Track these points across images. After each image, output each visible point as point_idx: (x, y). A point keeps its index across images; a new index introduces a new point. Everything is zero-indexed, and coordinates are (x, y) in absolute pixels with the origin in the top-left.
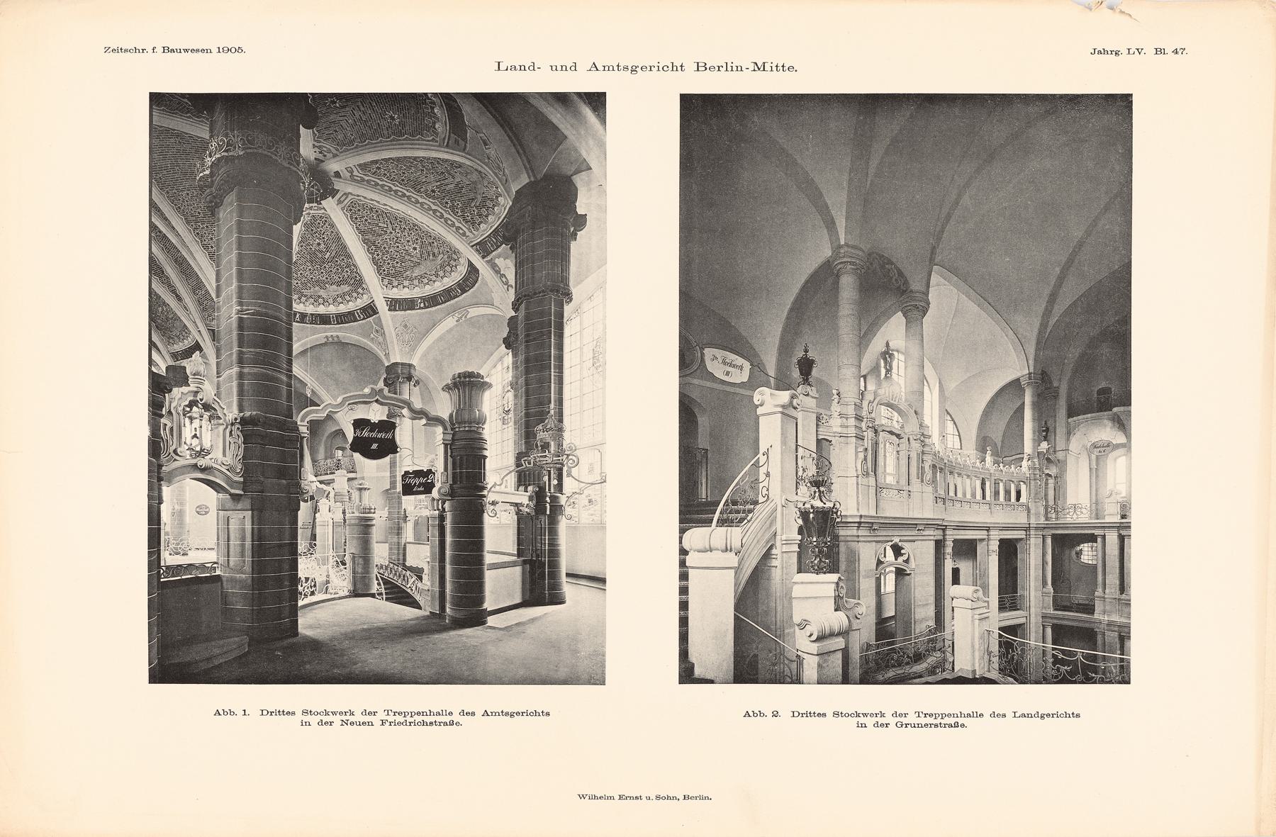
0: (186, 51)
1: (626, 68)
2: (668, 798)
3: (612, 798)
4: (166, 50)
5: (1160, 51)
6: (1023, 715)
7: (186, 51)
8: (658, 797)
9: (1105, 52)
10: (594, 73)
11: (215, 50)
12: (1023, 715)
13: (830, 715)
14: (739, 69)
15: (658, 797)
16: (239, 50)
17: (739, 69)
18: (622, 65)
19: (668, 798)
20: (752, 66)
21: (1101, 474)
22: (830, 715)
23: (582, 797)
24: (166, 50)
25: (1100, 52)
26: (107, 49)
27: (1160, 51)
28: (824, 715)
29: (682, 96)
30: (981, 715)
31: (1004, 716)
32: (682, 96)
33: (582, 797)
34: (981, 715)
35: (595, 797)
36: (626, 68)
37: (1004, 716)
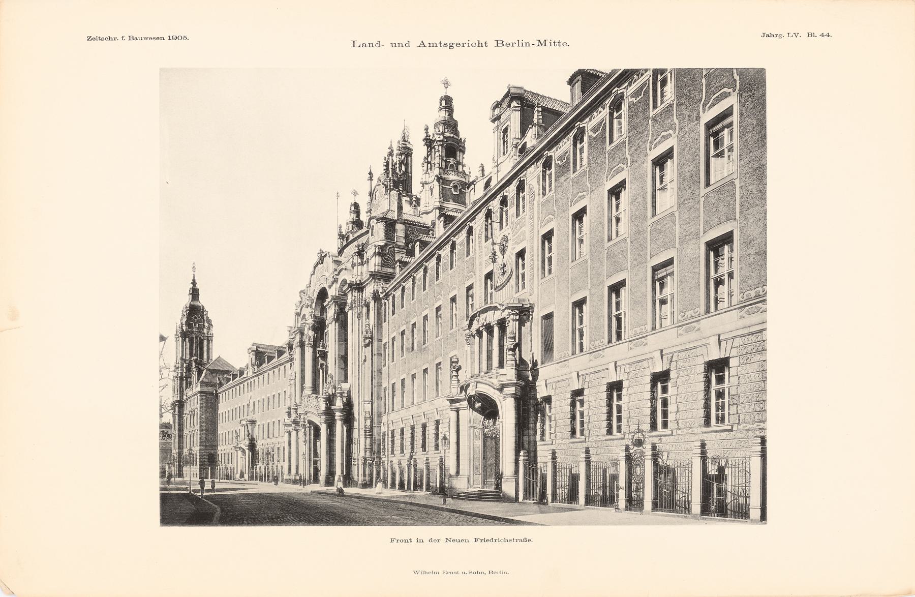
0: (146, 38)
1: (446, 45)
2: (478, 573)
7: (146, 38)
8: (471, 573)
10: (422, 48)
15: (471, 573)
18: (443, 43)
19: (478, 573)
20: (536, 43)
23: (416, 572)
26: (89, 38)
33: (416, 572)
36: (446, 45)
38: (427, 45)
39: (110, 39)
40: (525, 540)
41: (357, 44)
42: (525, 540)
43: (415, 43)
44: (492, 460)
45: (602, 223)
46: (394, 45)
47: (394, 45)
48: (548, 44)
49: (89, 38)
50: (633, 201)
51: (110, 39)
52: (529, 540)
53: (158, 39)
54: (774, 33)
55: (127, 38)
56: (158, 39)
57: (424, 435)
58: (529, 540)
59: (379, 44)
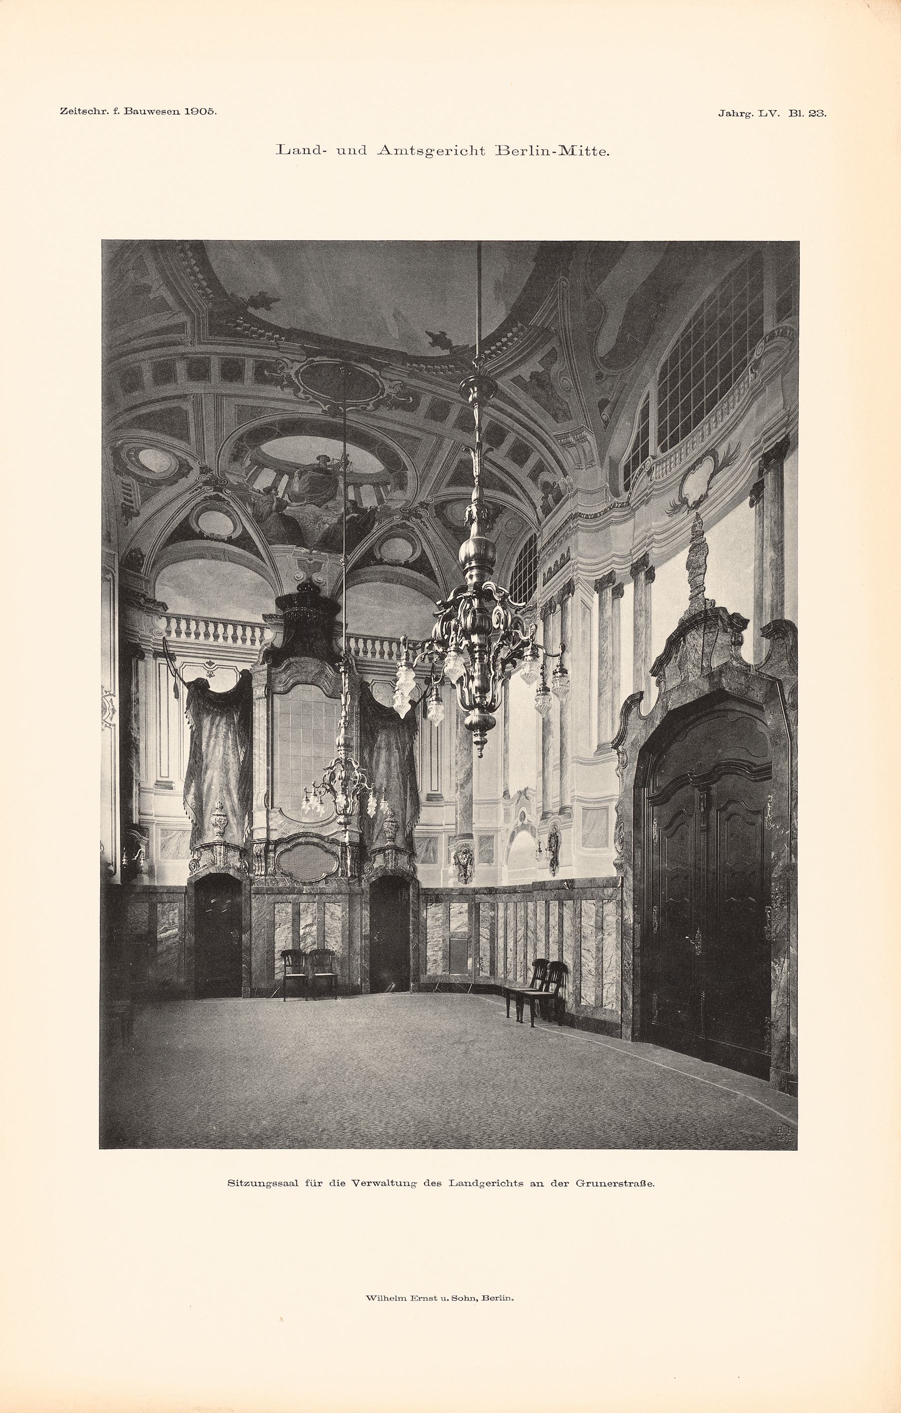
0: (151, 112)
1: (420, 152)
2: (466, 1298)
6: (460, 1184)
7: (151, 112)
8: (455, 1298)
12: (460, 1184)
13: (527, 1184)
14: (545, 152)
15: (455, 1298)
16: (210, 112)
17: (545, 152)
19: (466, 1298)
20: (559, 150)
22: (527, 1184)
23: (370, 1298)
26: (64, 111)
28: (439, 1184)
30: (521, 1184)
33: (370, 1298)
34: (521, 1184)
35: (386, 1298)
36: (420, 152)
38: (392, 151)
39: (95, 111)
41: (285, 150)
43: (374, 148)
46: (341, 152)
47: (341, 152)
48: (577, 151)
49: (64, 111)
50: (616, 686)
51: (95, 111)
55: (122, 110)
57: (493, 949)
59: (318, 150)
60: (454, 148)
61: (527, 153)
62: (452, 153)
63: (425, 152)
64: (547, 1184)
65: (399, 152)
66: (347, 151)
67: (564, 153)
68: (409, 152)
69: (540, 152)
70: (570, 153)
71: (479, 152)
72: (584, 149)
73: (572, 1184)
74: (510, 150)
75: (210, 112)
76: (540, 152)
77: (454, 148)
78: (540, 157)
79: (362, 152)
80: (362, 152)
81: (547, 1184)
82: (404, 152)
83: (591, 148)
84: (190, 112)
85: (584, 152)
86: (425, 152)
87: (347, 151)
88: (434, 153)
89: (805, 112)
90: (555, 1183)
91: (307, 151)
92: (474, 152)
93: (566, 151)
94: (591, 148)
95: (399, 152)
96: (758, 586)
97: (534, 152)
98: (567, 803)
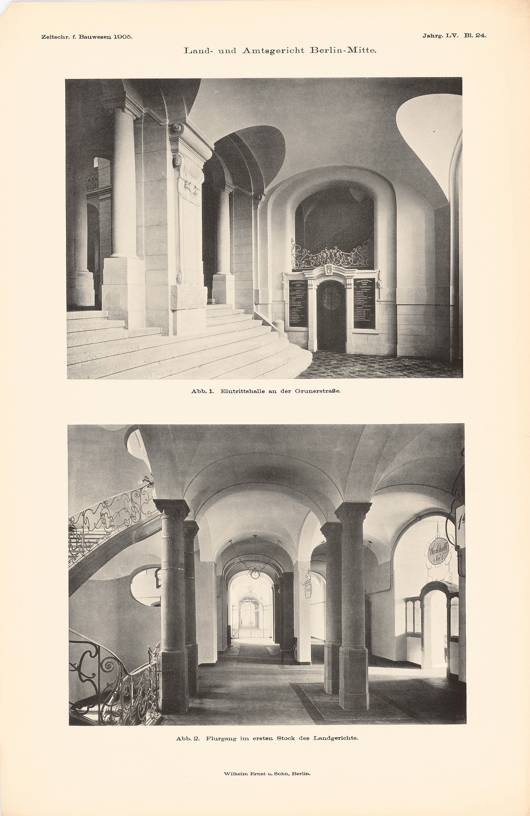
0: (94, 37)
1: (267, 51)
3: (246, 774)
4: (82, 37)
5: (467, 35)
7: (94, 37)
8: (276, 774)
9: (432, 36)
10: (247, 54)
11: (113, 37)
13: (267, 392)
15: (276, 774)
16: (128, 37)
20: (348, 50)
21: (220, 494)
22: (267, 392)
24: (82, 37)
25: (429, 36)
27: (467, 35)
29: (72, 86)
31: (308, 739)
32: (72, 86)
34: (263, 392)
36: (267, 51)
37: (308, 739)
39: (62, 37)
40: (334, 391)
41: (189, 51)
42: (334, 391)
43: (240, 49)
44: (183, 606)
45: (447, 339)
46: (221, 52)
47: (221, 52)
48: (357, 50)
51: (62, 37)
52: (355, 738)
53: (102, 37)
54: (434, 34)
56: (102, 37)
58: (355, 738)
60: (286, 49)
61: (329, 52)
62: (285, 52)
63: (270, 51)
64: (278, 392)
65: (255, 52)
66: (225, 52)
67: (350, 51)
68: (261, 51)
69: (336, 51)
70: (354, 51)
71: (301, 51)
72: (361, 49)
73: (293, 392)
74: (319, 50)
75: (128, 37)
76: (336, 51)
77: (286, 49)
78: (228, 54)
79: (207, 52)
80: (207, 52)
81: (278, 392)
82: (258, 51)
83: (365, 48)
84: (117, 37)
85: (362, 51)
86: (270, 51)
87: (225, 52)
88: (275, 52)
89: (474, 35)
90: (283, 391)
91: (201, 52)
92: (298, 51)
93: (353, 50)
94: (365, 48)
95: (255, 52)
96: (113, 216)
97: (333, 51)
98: (332, 274)
